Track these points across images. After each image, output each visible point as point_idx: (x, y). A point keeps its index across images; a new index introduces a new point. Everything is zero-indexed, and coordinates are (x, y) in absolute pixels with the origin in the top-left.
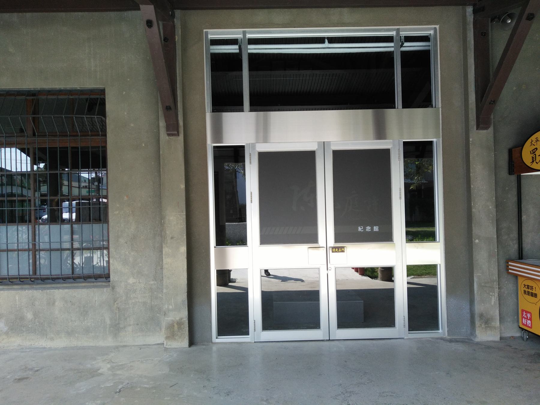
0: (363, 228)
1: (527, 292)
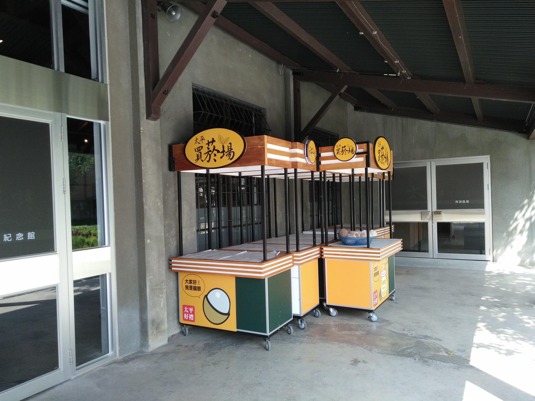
0: (10, 237)
1: (189, 287)
